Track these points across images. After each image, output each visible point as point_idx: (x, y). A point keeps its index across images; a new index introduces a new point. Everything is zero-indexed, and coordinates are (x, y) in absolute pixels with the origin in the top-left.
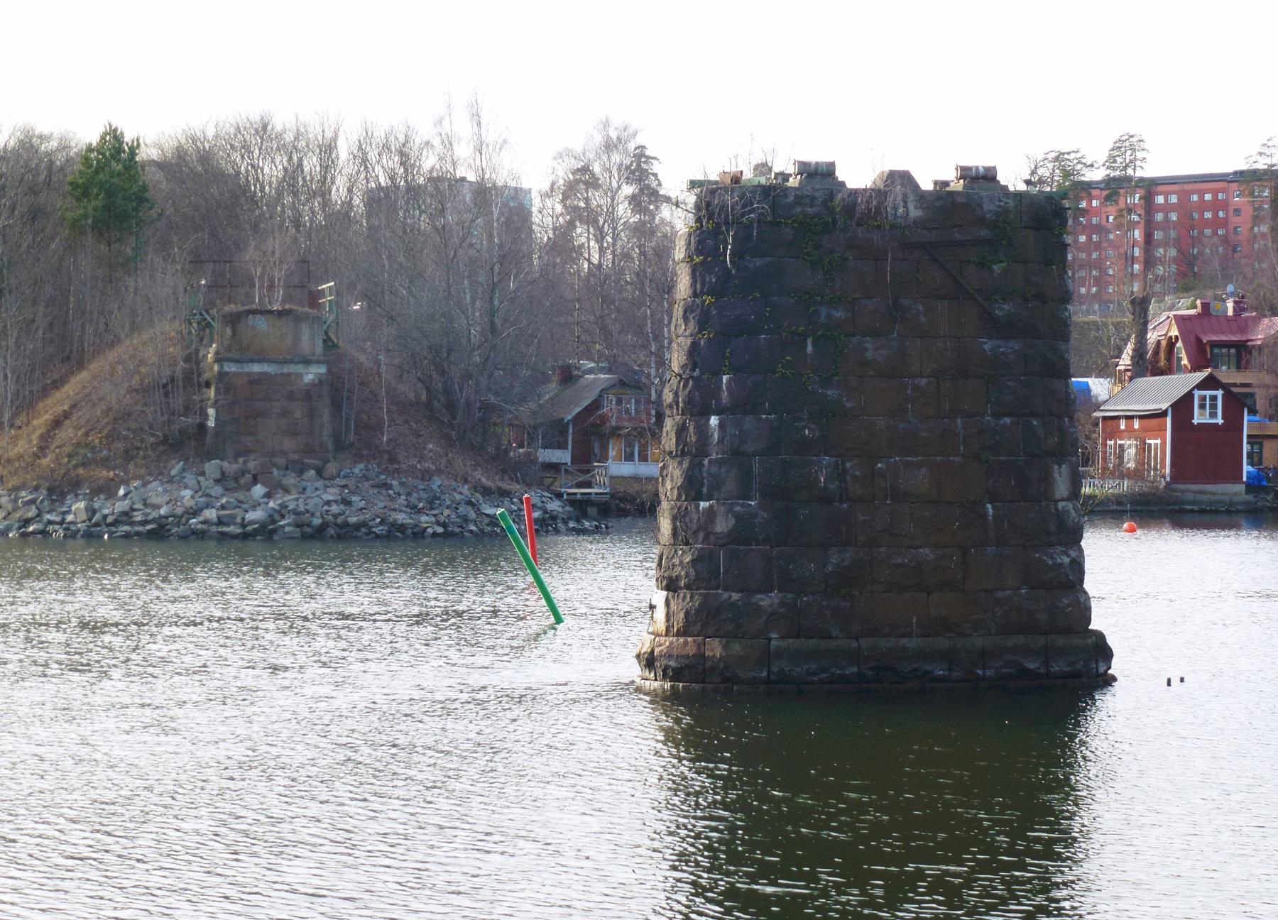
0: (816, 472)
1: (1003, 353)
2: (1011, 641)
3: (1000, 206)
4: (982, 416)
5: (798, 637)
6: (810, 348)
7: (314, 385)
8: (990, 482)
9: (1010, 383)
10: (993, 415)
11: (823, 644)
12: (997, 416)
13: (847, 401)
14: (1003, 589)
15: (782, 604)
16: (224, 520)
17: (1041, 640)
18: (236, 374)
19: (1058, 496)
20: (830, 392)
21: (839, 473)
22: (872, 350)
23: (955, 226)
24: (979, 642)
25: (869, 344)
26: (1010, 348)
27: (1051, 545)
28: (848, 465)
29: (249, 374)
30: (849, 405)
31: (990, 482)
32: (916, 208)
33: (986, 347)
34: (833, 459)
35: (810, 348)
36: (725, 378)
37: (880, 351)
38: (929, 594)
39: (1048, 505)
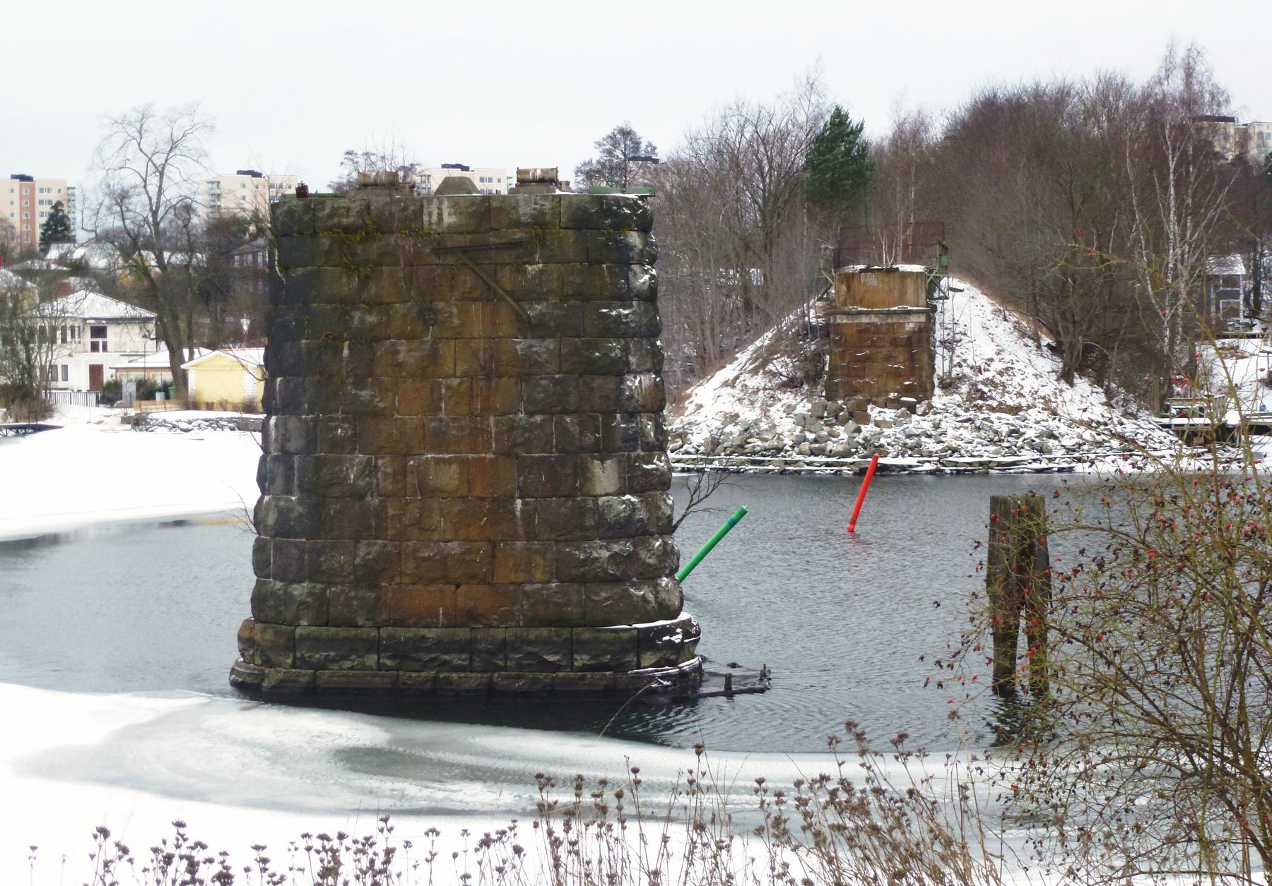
0: (348, 469)
1: (536, 353)
2: (533, 633)
3: (535, 209)
4: (516, 413)
5: (326, 625)
6: (346, 352)
7: (914, 332)
8: (521, 478)
9: (543, 382)
10: (526, 412)
11: (343, 632)
12: (530, 414)
13: (380, 401)
14: (531, 582)
15: (311, 594)
16: (816, 452)
17: (565, 633)
18: (846, 324)
19: (599, 490)
20: (363, 393)
21: (370, 469)
22: (407, 353)
23: (492, 229)
24: (500, 634)
25: (403, 346)
26: (544, 347)
27: (588, 539)
28: (380, 462)
29: (858, 325)
30: (381, 405)
31: (521, 478)
32: (450, 214)
33: (518, 347)
34: (367, 457)
35: (346, 352)
36: (279, 380)
37: (413, 354)
38: (458, 586)
39: (584, 501)
